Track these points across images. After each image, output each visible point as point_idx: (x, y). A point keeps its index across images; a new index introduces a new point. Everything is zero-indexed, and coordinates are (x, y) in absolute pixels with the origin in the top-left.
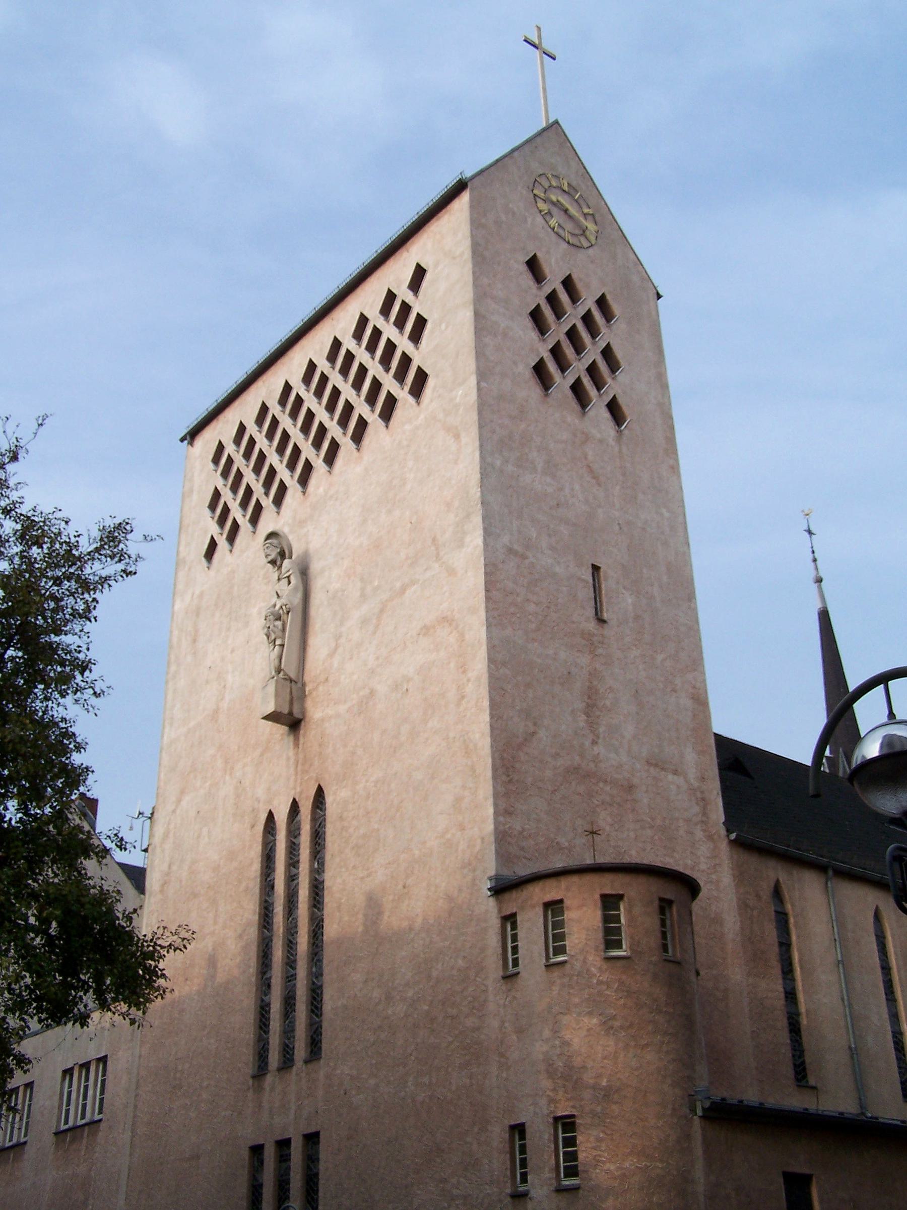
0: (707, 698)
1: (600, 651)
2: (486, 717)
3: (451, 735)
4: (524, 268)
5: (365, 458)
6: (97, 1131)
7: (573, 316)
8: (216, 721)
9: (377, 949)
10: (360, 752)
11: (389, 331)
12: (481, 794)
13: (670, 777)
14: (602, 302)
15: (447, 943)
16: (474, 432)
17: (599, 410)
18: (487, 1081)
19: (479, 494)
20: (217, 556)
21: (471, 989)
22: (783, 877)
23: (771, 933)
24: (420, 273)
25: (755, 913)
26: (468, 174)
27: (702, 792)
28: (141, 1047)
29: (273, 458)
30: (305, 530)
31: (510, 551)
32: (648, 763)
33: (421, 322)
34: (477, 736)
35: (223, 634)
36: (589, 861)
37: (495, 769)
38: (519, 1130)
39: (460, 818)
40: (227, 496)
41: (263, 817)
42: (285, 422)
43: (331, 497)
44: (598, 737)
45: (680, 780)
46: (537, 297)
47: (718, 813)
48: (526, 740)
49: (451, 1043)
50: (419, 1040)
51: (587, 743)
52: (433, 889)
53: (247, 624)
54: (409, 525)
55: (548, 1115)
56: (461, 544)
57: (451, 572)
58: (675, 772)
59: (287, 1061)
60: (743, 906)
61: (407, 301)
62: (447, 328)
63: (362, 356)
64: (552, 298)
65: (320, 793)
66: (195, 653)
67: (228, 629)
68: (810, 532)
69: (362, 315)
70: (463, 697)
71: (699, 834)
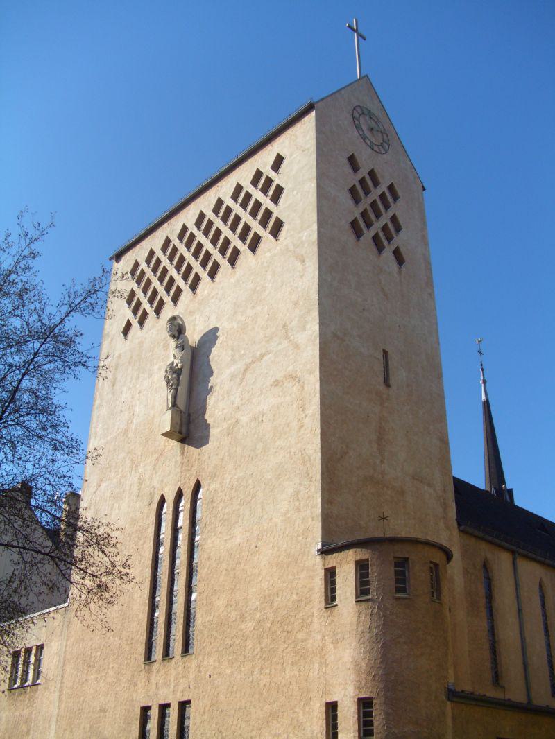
0: (448, 440)
1: (386, 404)
2: (318, 440)
3: (293, 450)
4: (346, 161)
5: (238, 273)
6: (36, 690)
7: (375, 194)
8: (127, 436)
9: (235, 586)
10: (227, 459)
11: (257, 195)
12: (313, 489)
13: (426, 487)
14: (391, 188)
15: (285, 585)
16: (315, 258)
17: (388, 253)
18: (311, 674)
19: (317, 298)
20: (131, 333)
21: (301, 614)
22: (489, 556)
23: (482, 591)
24: (279, 160)
25: (473, 577)
26: (315, 100)
27: (444, 499)
28: (67, 640)
29: (173, 272)
30: (194, 317)
31: (335, 335)
32: (413, 478)
33: (279, 190)
34: (311, 452)
35: (134, 381)
36: (378, 534)
37: (322, 474)
38: (332, 708)
39: (297, 504)
40: (139, 294)
41: (157, 498)
42: (182, 249)
43: (213, 297)
44: (384, 459)
45: (431, 490)
46: (354, 180)
47: (453, 513)
48: (342, 457)
49: (287, 648)
50: (263, 645)
51: (378, 462)
52: (276, 548)
53: (150, 375)
54: (267, 316)
55: (354, 697)
56: (304, 329)
57: (297, 346)
58: (429, 485)
59: (167, 654)
60: (466, 572)
61: (270, 176)
62: (297, 193)
63: (165, 262)
64: (362, 181)
65: (198, 486)
66: (114, 393)
67: (138, 378)
68: (481, 353)
69: (136, 261)
70: (302, 426)
71: (441, 524)
